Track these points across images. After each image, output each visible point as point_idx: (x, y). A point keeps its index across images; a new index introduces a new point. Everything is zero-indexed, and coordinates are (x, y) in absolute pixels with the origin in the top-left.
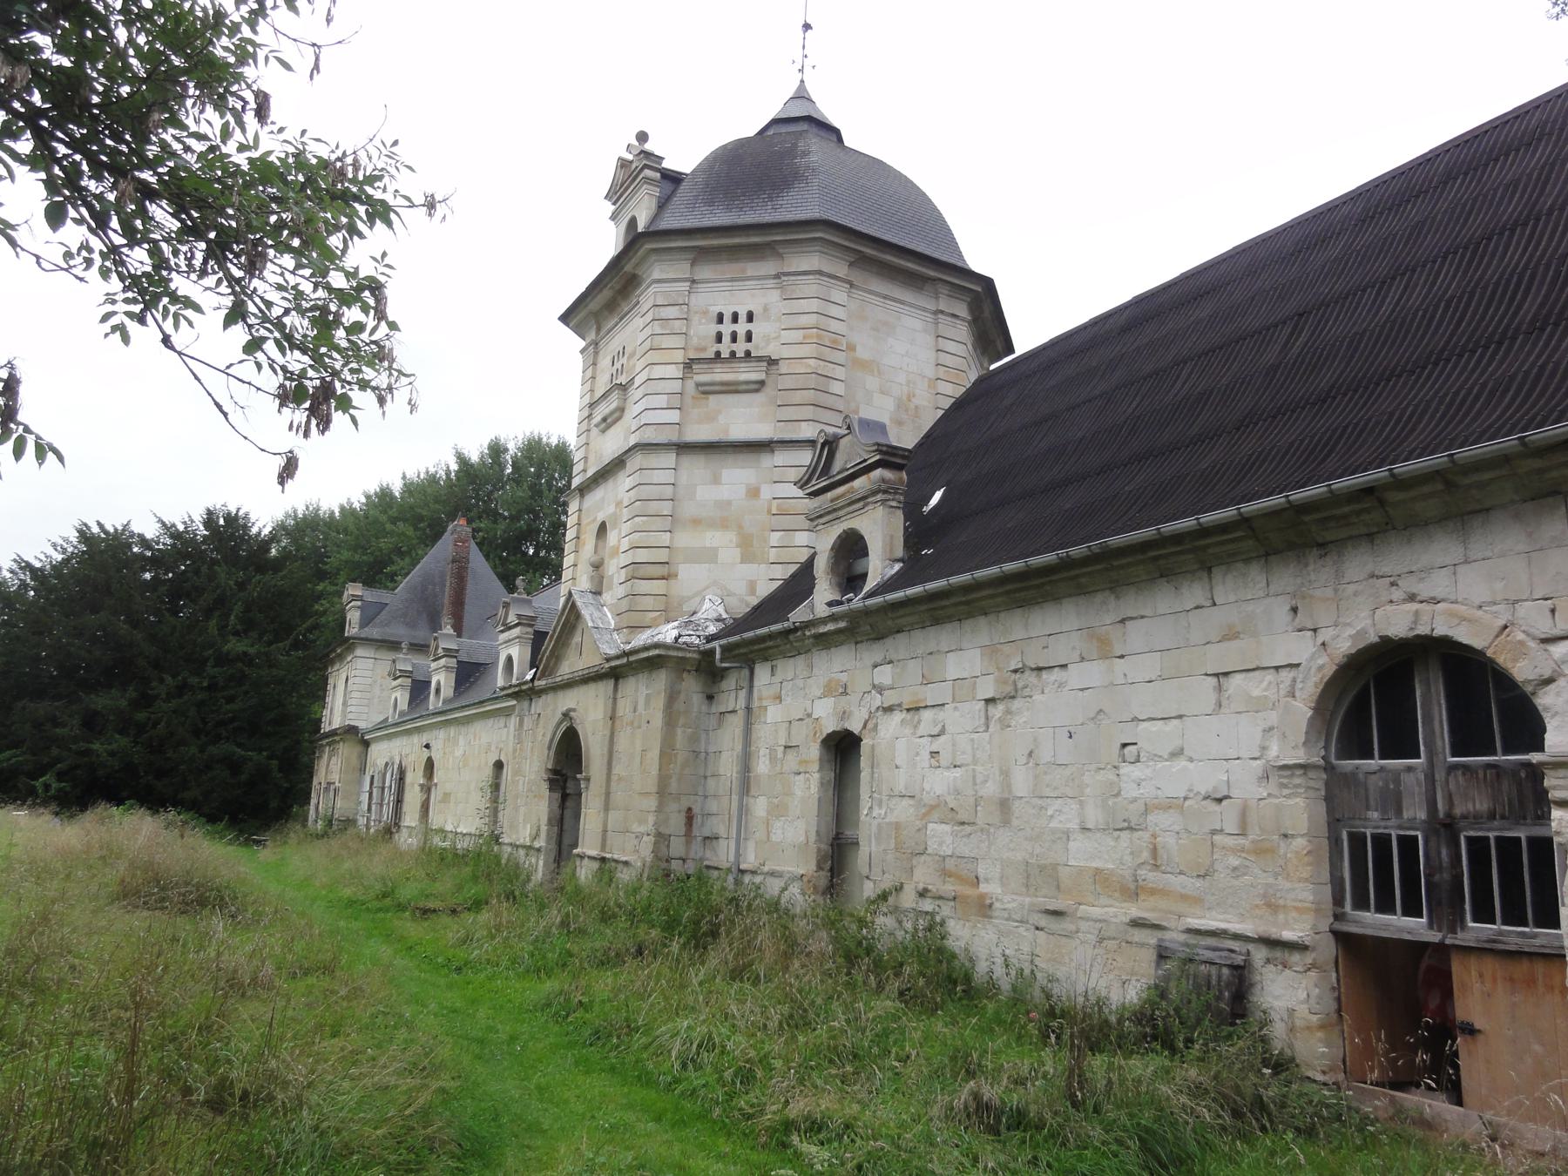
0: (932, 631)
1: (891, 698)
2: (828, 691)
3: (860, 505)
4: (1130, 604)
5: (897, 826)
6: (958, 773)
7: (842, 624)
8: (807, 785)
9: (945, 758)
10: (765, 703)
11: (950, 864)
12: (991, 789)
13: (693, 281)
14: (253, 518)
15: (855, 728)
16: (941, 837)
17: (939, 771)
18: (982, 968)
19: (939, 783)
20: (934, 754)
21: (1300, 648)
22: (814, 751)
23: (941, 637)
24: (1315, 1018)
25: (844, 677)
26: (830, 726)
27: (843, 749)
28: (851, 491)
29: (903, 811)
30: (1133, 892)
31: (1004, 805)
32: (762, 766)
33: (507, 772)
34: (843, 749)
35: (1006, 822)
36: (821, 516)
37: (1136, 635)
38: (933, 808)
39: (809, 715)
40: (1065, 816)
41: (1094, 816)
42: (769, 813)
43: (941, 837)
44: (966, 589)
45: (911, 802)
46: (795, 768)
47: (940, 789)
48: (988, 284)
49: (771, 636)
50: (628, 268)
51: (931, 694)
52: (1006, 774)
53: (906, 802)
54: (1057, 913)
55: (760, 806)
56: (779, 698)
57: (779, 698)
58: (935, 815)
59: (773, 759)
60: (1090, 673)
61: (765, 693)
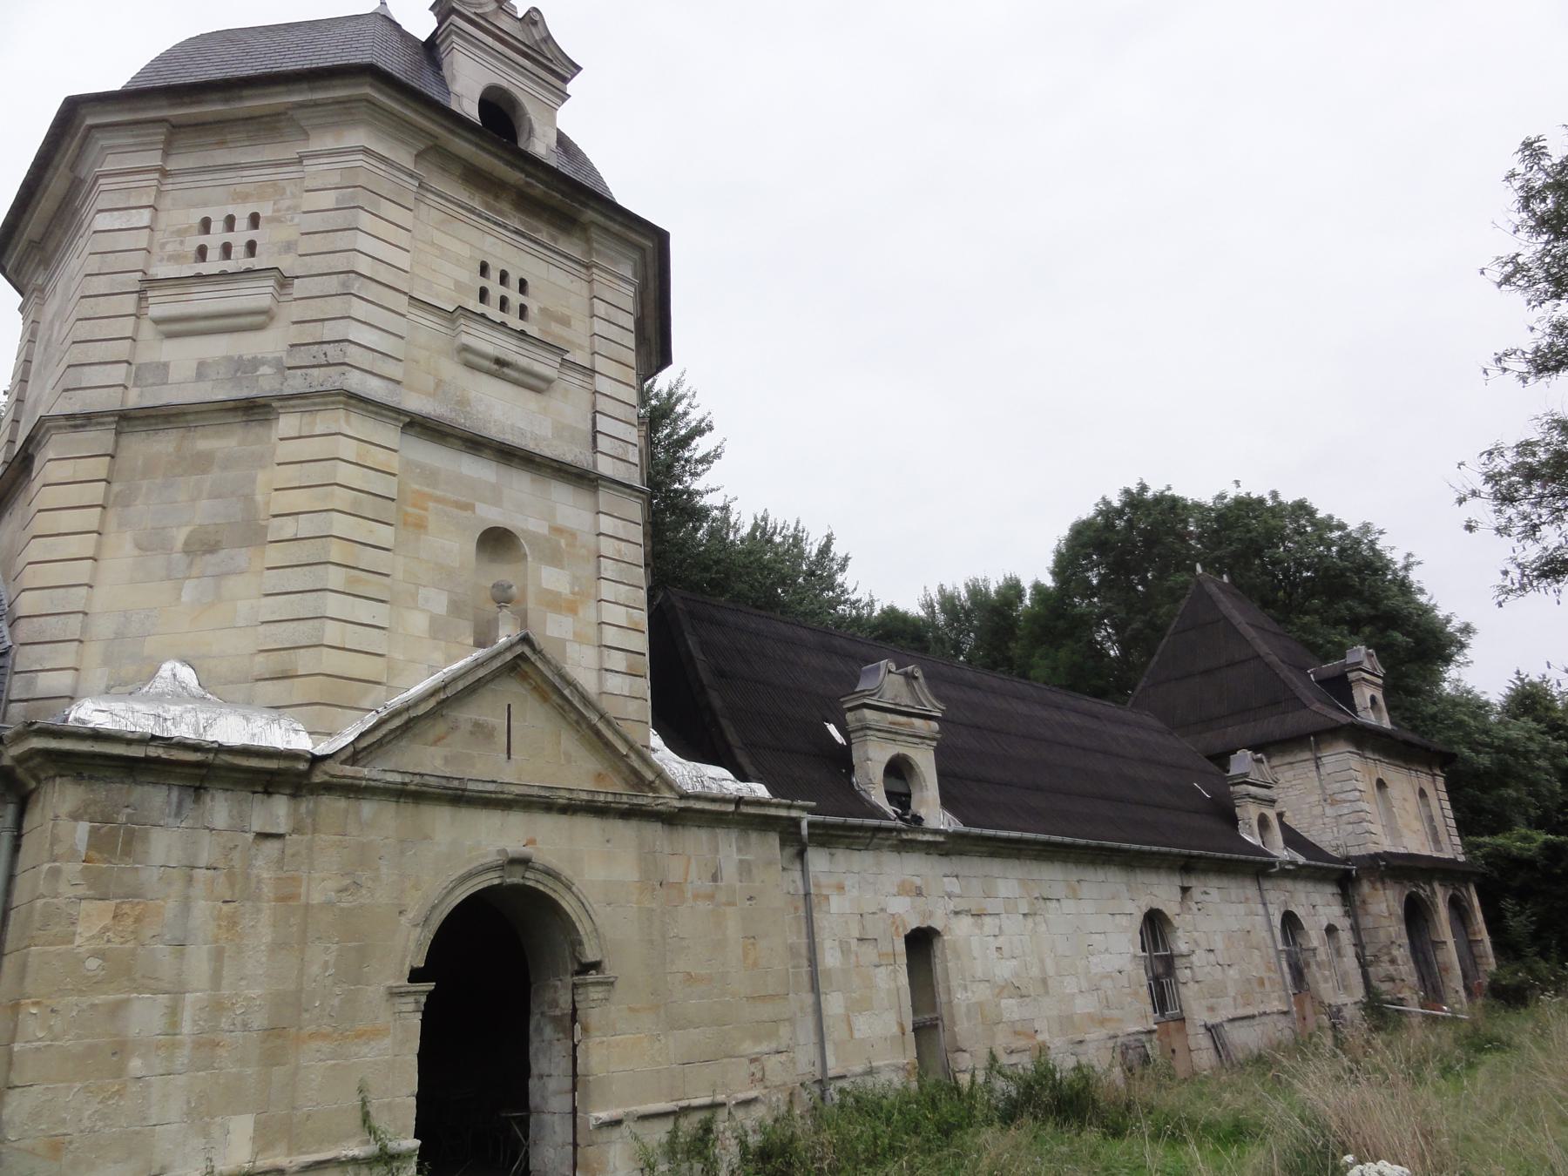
0: (987, 861)
1: (962, 904)
4: (1319, 887)
5: (980, 1004)
6: (1014, 962)
7: (940, 839)
8: (894, 979)
11: (1018, 1027)
12: (1035, 972)
13: (164, 173)
16: (1011, 1008)
19: (1005, 970)
21: (1130, 907)
23: (995, 867)
25: (918, 881)
26: (914, 923)
27: (921, 943)
28: (911, 726)
29: (981, 993)
30: (1103, 1022)
31: (1044, 981)
32: (830, 958)
33: (946, 961)
34: (921, 943)
35: (1047, 993)
37: (1086, 890)
39: (882, 910)
40: (1070, 985)
41: (1085, 986)
43: (1011, 1008)
44: (1112, 850)
46: (876, 960)
49: (861, 828)
52: (1042, 961)
53: (982, 986)
54: (1081, 1042)
55: (834, 1004)
56: (841, 888)
57: (841, 888)
59: (845, 950)
60: (1069, 906)
61: (824, 880)
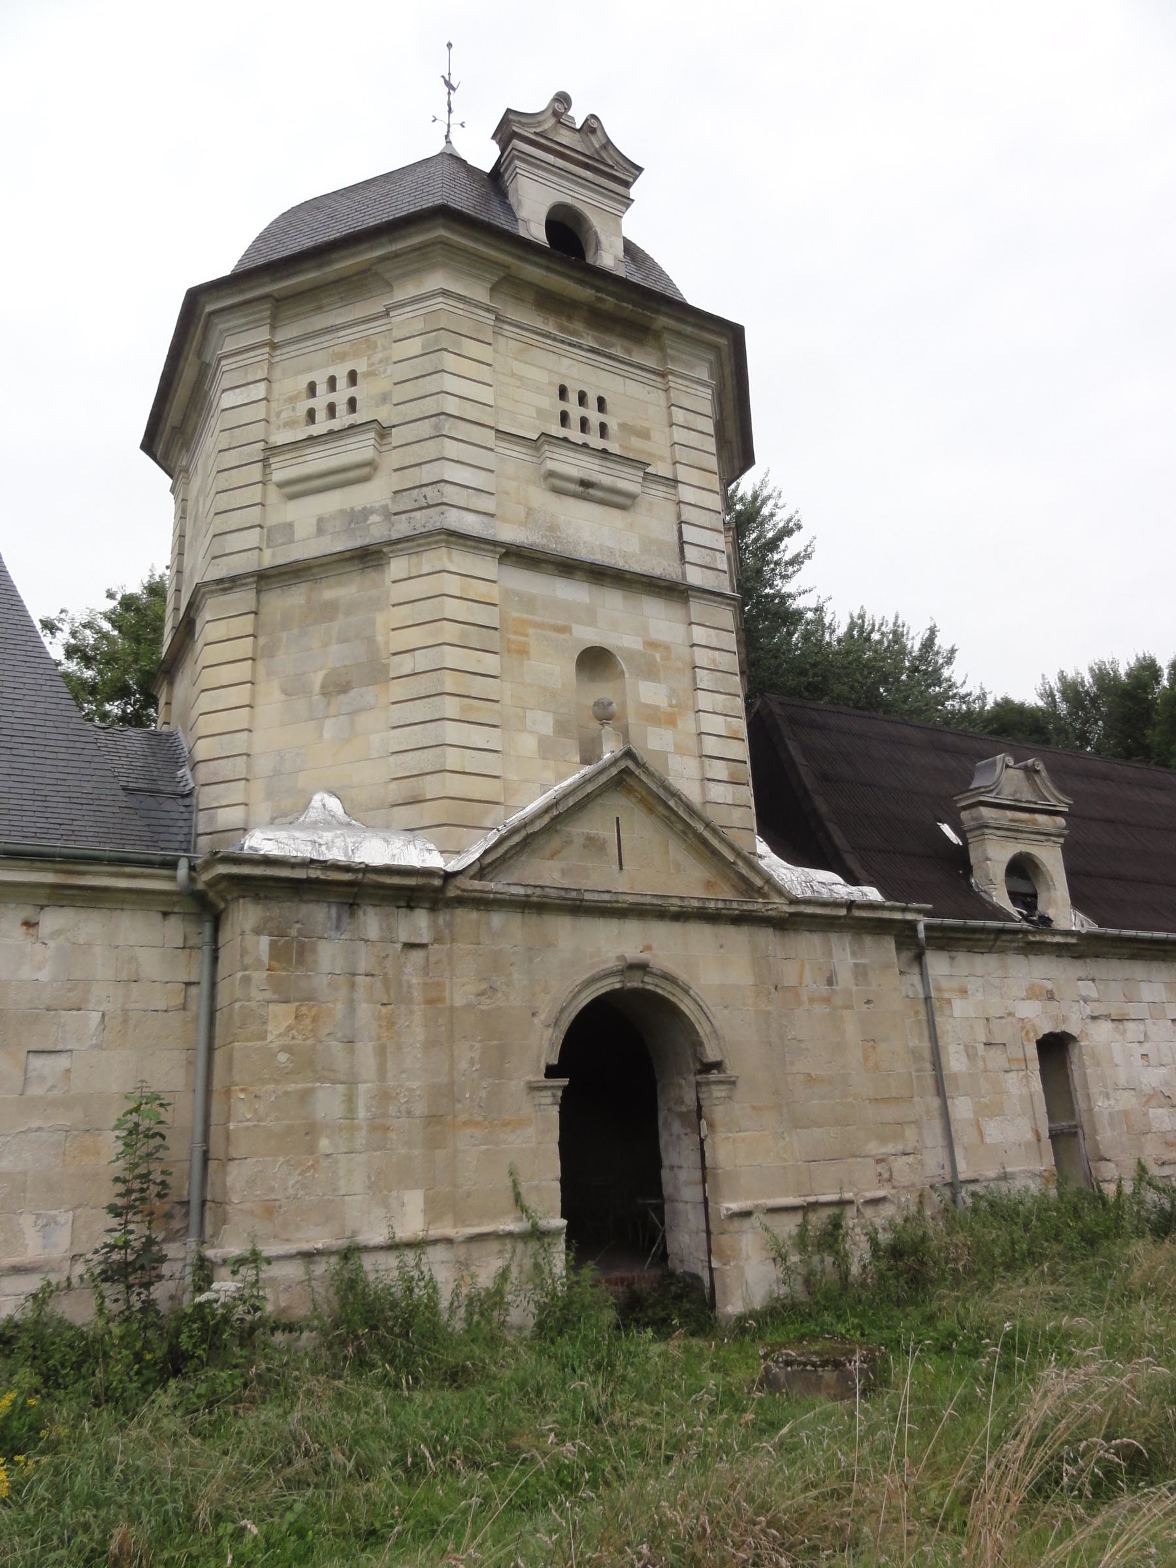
0: (1127, 963)
1: (1099, 1009)
2: (1032, 994)
3: (1042, 838)
5: (1126, 1114)
7: (1073, 941)
8: (1025, 1084)
9: (1153, 1059)
10: (946, 995)
14: (1070, 675)
15: (1073, 1030)
17: (1150, 1069)
18: (18, 1317)
19: (1152, 1078)
20: (1144, 1056)
22: (1032, 1051)
23: (1137, 970)
24: (80, 1268)
26: (1046, 1028)
27: (1055, 1049)
28: (1034, 822)
29: (1127, 1101)
32: (955, 1062)
36: (998, 829)
38: (1152, 1096)
42: (976, 1113)
45: (1132, 1093)
47: (1155, 1082)
48: (195, 298)
49: (983, 930)
50: (662, 321)
51: (1132, 1010)
55: (962, 1108)
58: (1154, 1102)
61: (944, 984)
